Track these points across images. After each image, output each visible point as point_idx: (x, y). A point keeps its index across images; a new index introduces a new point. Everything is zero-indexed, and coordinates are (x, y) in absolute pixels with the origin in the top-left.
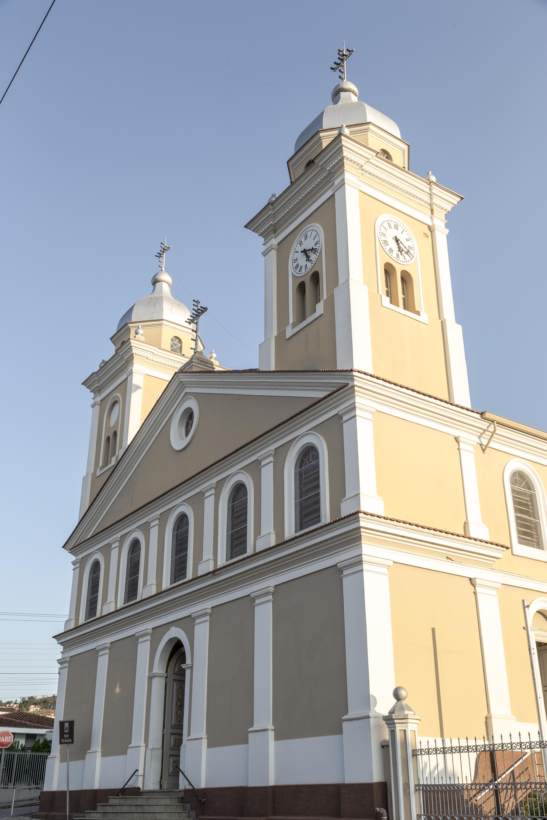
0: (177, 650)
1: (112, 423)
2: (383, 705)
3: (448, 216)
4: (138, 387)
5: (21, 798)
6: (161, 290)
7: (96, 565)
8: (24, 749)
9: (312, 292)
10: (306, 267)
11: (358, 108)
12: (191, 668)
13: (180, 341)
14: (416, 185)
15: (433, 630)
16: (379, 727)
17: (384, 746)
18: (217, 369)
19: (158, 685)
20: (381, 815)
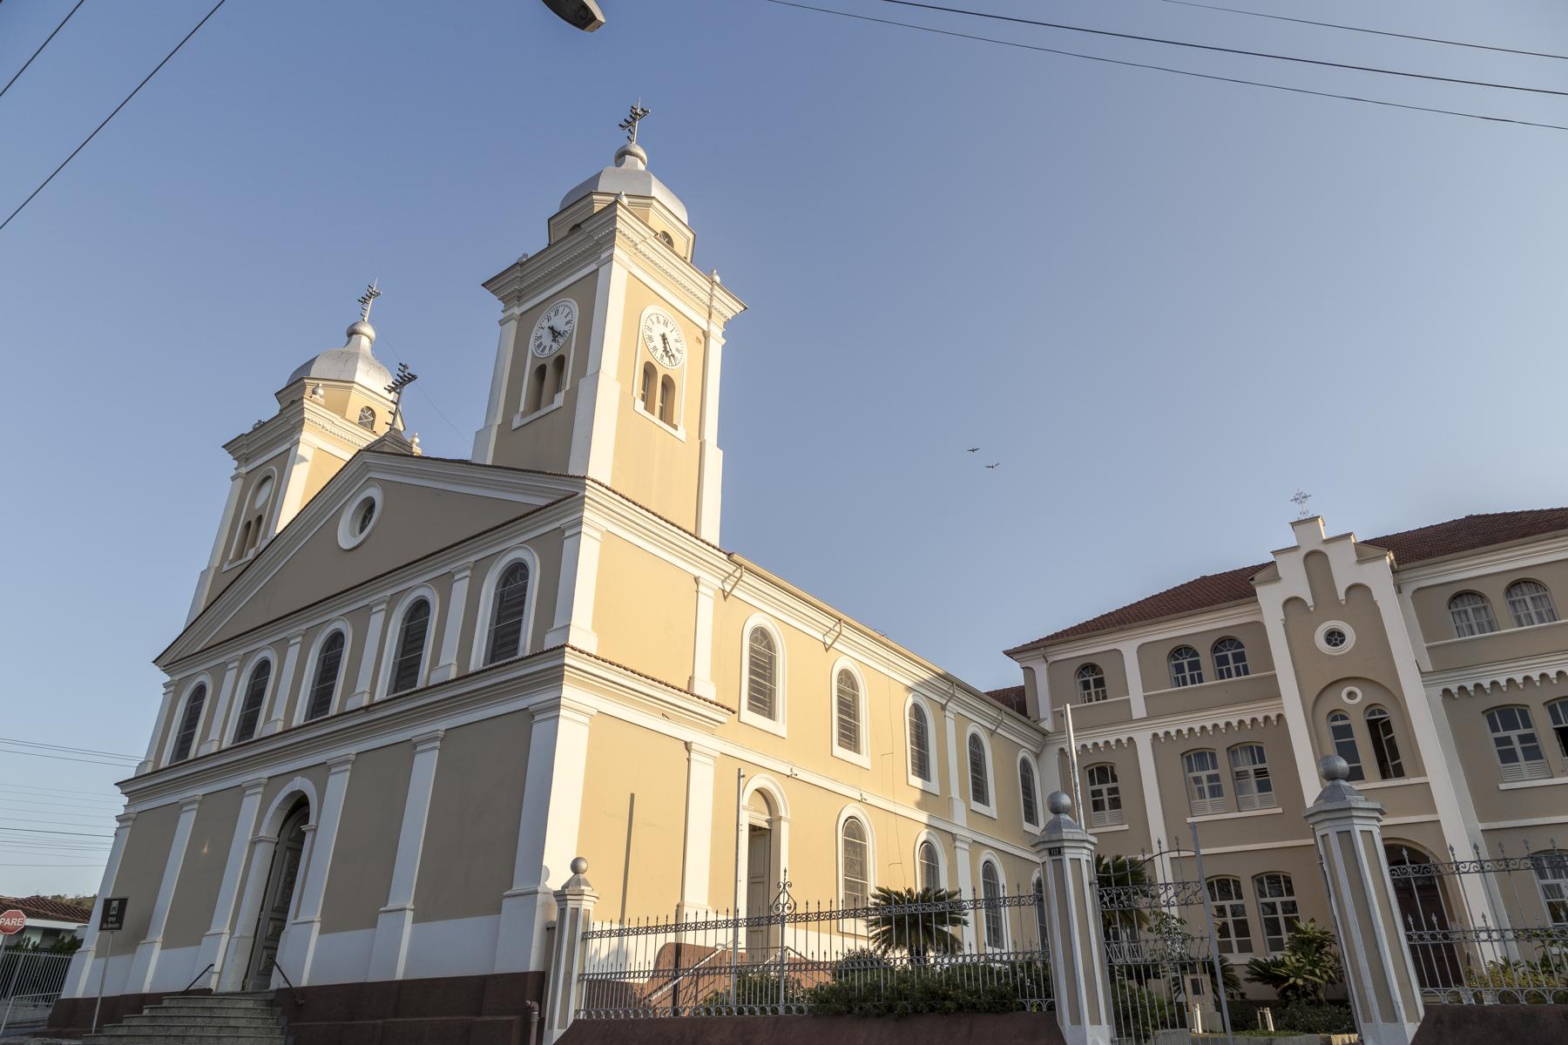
0: (298, 808)
1: (258, 504)
2: (557, 875)
3: (727, 324)
4: (303, 459)
5: (19, 1018)
6: (359, 345)
7: (200, 691)
8: (36, 949)
9: (552, 381)
10: (552, 348)
11: (643, 178)
12: (315, 830)
13: (373, 414)
14: (697, 282)
15: (632, 796)
16: (547, 905)
17: (550, 929)
18: (417, 450)
19: (263, 854)
20: (531, 1009)
